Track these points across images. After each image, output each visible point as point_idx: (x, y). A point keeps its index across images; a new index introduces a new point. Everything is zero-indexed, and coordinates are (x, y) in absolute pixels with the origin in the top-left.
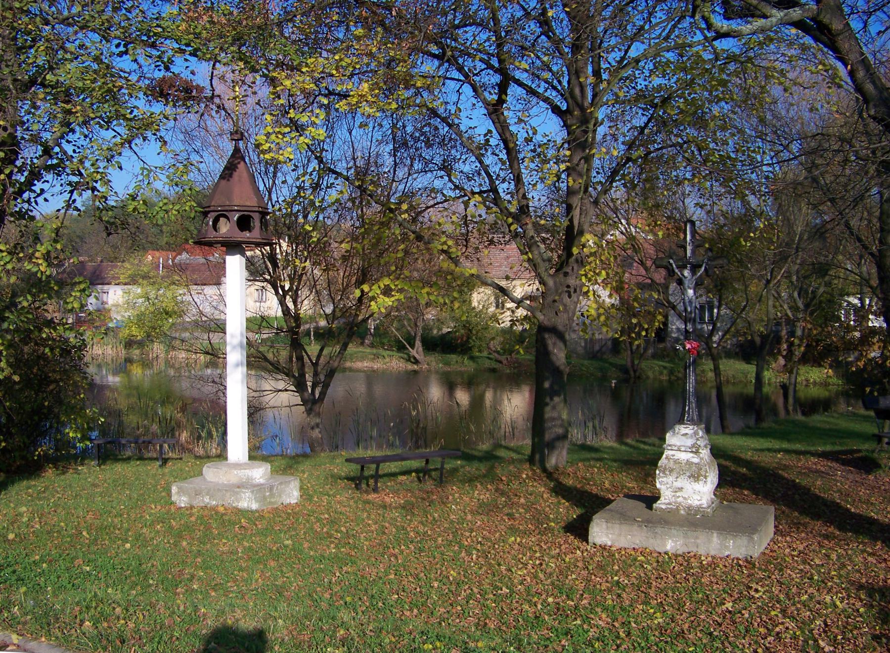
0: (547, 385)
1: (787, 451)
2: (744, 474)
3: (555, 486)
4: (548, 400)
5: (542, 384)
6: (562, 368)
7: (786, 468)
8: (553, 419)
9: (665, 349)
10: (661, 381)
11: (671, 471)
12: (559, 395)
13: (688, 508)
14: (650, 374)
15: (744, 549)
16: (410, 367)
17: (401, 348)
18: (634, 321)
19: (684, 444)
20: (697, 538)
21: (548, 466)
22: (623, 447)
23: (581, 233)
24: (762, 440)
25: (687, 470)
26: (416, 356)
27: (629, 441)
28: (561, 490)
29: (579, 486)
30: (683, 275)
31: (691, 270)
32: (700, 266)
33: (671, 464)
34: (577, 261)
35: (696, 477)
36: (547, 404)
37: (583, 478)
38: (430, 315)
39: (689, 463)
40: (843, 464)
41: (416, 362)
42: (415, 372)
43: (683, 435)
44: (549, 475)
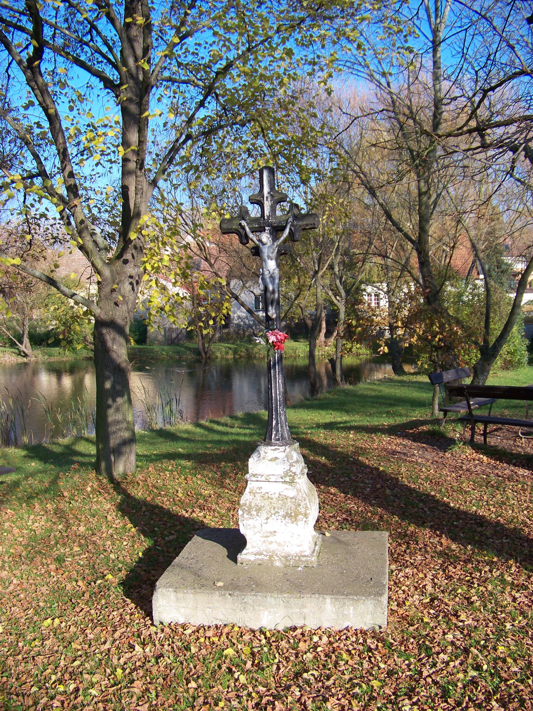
0: (108, 385)
1: (359, 429)
2: (324, 465)
3: (123, 501)
4: (110, 402)
5: (103, 384)
6: (124, 365)
7: (363, 451)
8: (118, 422)
9: (228, 334)
10: (227, 360)
11: (259, 510)
12: (123, 396)
13: (286, 557)
14: (219, 355)
15: (369, 617)
16: (21, 360)
17: (13, 345)
18: (201, 310)
19: (276, 475)
20: (303, 606)
21: (115, 474)
22: (198, 430)
23: (138, 215)
24: (323, 413)
25: (278, 502)
26: (25, 350)
27: (203, 422)
28: (130, 508)
29: (149, 499)
30: (260, 241)
31: (271, 234)
32: (283, 229)
33: (258, 501)
34: (135, 247)
35: (292, 516)
36: (109, 407)
37: (154, 486)
38: (36, 314)
39: (283, 498)
40: (414, 440)
41: (26, 355)
42: (26, 364)
43: (271, 460)
44: (117, 485)
